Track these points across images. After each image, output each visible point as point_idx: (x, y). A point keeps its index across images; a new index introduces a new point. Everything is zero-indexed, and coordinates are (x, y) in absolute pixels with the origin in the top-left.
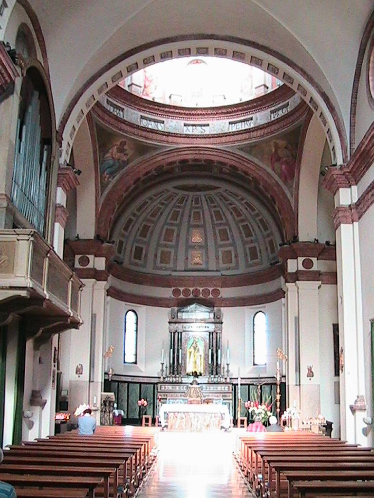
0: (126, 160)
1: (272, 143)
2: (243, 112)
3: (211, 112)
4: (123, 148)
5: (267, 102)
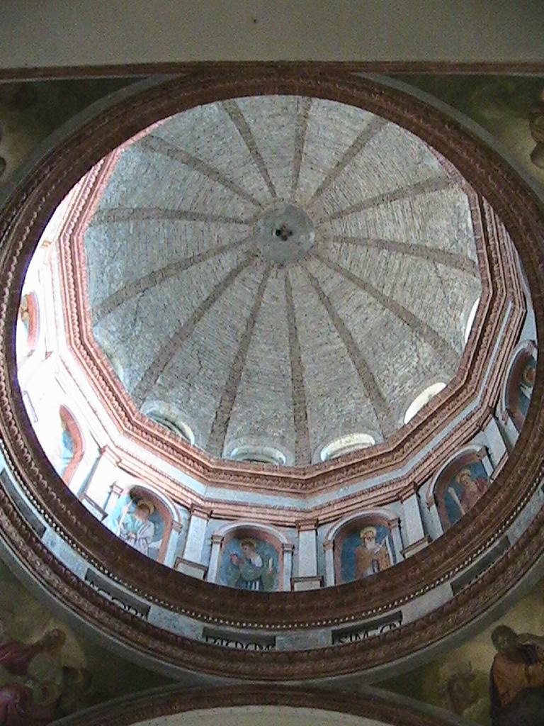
1: (52, 626)
2: (39, 497)
3: (9, 408)
5: (97, 547)
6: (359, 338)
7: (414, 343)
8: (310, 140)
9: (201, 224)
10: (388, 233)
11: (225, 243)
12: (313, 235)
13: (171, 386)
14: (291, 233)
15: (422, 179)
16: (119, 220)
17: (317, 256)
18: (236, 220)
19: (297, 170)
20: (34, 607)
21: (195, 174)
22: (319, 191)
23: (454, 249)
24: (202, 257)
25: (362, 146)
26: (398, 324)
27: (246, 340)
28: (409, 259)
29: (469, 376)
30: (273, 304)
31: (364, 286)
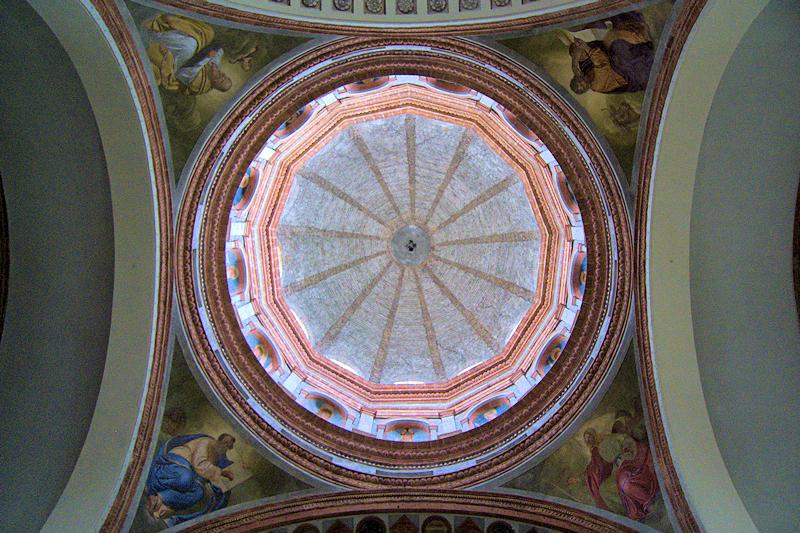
0: (224, 490)
1: (581, 439)
4: (224, 455)
6: (474, 195)
7: (470, 158)
8: (344, 228)
9: (400, 302)
10: (404, 176)
11: (415, 286)
12: (411, 227)
13: (500, 329)
14: (411, 241)
15: (360, 155)
16: (385, 357)
17: (426, 223)
18: (400, 279)
19: (366, 237)
20: (564, 450)
21: (364, 305)
22: (380, 222)
23: (404, 133)
24: (423, 302)
25: (344, 194)
26: (461, 169)
27: (478, 273)
28: (418, 162)
29: (470, 119)
30: (464, 255)
31: (441, 191)
